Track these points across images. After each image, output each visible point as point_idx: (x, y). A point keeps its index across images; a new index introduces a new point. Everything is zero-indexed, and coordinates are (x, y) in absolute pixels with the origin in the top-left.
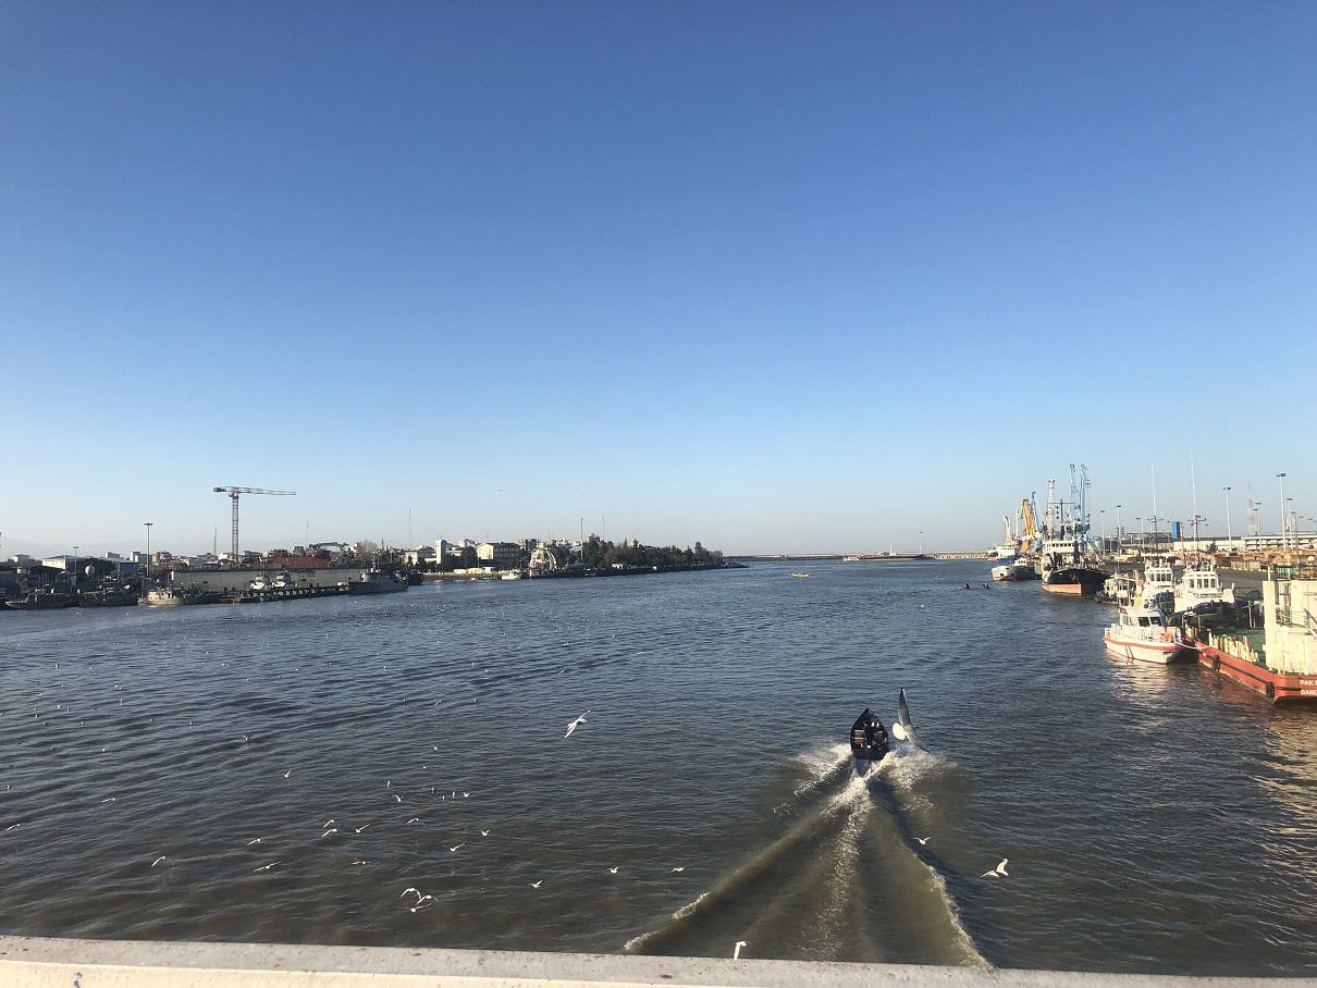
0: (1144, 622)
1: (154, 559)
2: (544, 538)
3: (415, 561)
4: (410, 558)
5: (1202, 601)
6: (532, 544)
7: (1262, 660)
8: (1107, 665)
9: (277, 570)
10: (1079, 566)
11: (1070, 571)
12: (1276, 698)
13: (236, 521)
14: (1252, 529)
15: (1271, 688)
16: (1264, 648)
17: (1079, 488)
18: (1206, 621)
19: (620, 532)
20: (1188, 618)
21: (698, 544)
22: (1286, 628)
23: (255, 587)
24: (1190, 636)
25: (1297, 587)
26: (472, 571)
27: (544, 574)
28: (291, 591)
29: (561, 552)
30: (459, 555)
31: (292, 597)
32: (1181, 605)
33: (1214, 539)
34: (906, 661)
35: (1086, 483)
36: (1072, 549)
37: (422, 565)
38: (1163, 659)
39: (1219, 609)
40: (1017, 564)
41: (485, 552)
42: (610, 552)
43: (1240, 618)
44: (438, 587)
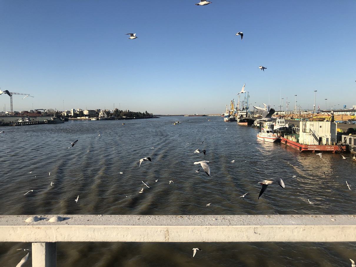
0: (268, 132)
2: (103, 109)
3: (66, 115)
4: (64, 114)
5: (281, 127)
6: (99, 111)
7: (298, 141)
8: (257, 144)
10: (247, 118)
11: (245, 119)
12: (302, 151)
13: (11, 102)
14: (287, 109)
15: (301, 148)
16: (299, 138)
18: (282, 132)
19: (124, 108)
21: (146, 112)
22: (305, 133)
23: (19, 121)
25: (308, 123)
26: (82, 118)
27: (103, 119)
28: (30, 123)
29: (108, 113)
31: (31, 124)
32: (275, 128)
34: (36, 146)
35: (249, 96)
36: (245, 114)
37: (68, 116)
38: (273, 141)
40: (230, 117)
41: (86, 112)
42: (122, 113)
43: (290, 131)
44: (72, 122)
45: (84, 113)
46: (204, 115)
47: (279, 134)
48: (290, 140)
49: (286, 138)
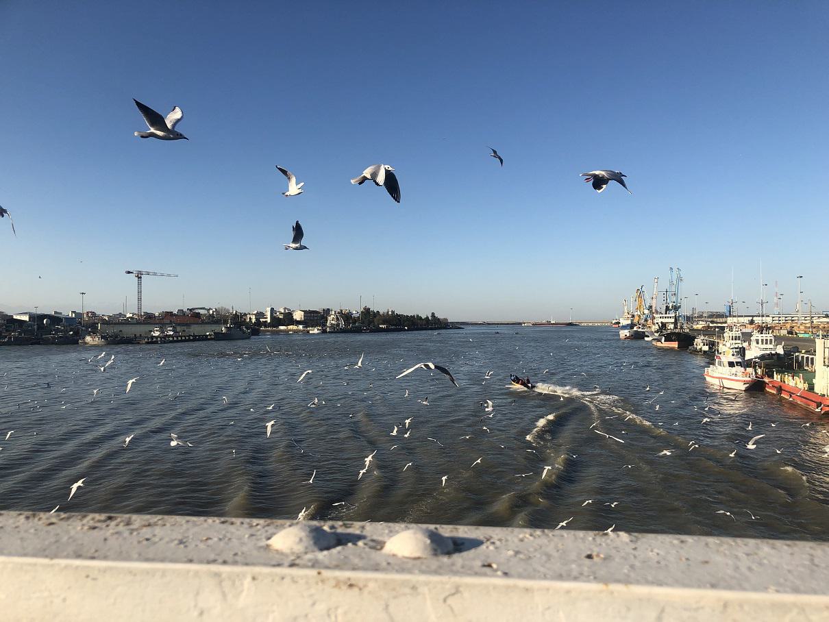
0: (731, 364)
1: (85, 316)
3: (254, 320)
4: (250, 318)
6: (327, 312)
7: (811, 388)
10: (677, 331)
13: (140, 292)
14: (776, 310)
16: (814, 381)
17: (675, 282)
18: (767, 365)
19: (382, 305)
20: (755, 362)
21: (433, 314)
23: (154, 335)
24: (759, 373)
26: (290, 327)
27: (336, 330)
28: (177, 337)
29: (347, 317)
30: (281, 317)
31: (177, 341)
32: (749, 355)
33: (753, 316)
35: (680, 279)
36: (673, 320)
37: (258, 323)
38: (743, 387)
39: (775, 357)
41: (298, 316)
45: (294, 318)
46: (570, 324)
47: (759, 371)
48: (791, 384)
49: (779, 380)
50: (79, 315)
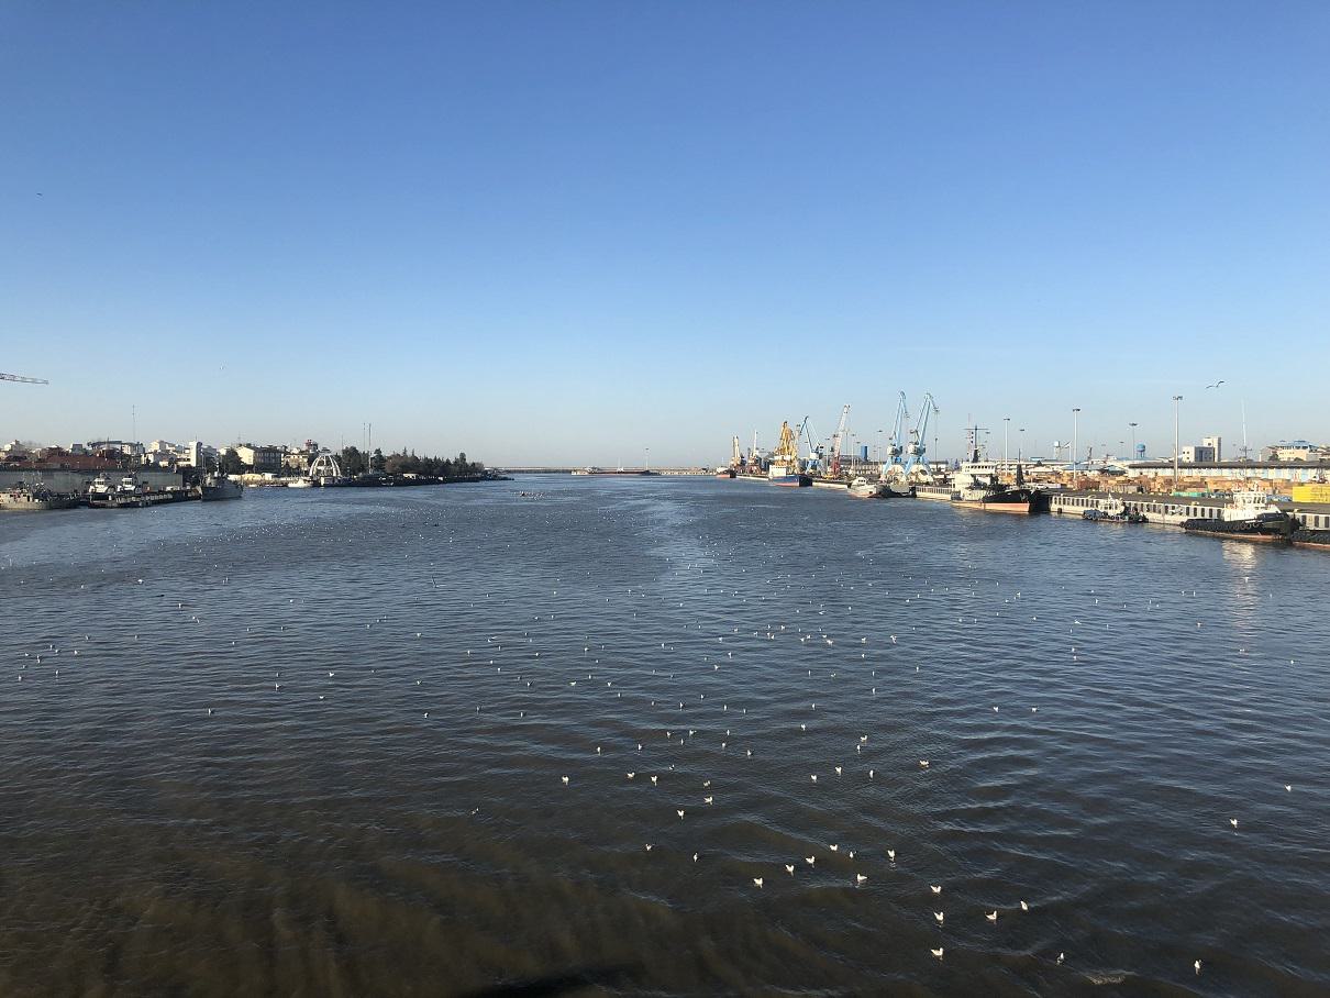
9: (55, 470)
41: (247, 456)
46: (647, 473)
50: (481, 465)
